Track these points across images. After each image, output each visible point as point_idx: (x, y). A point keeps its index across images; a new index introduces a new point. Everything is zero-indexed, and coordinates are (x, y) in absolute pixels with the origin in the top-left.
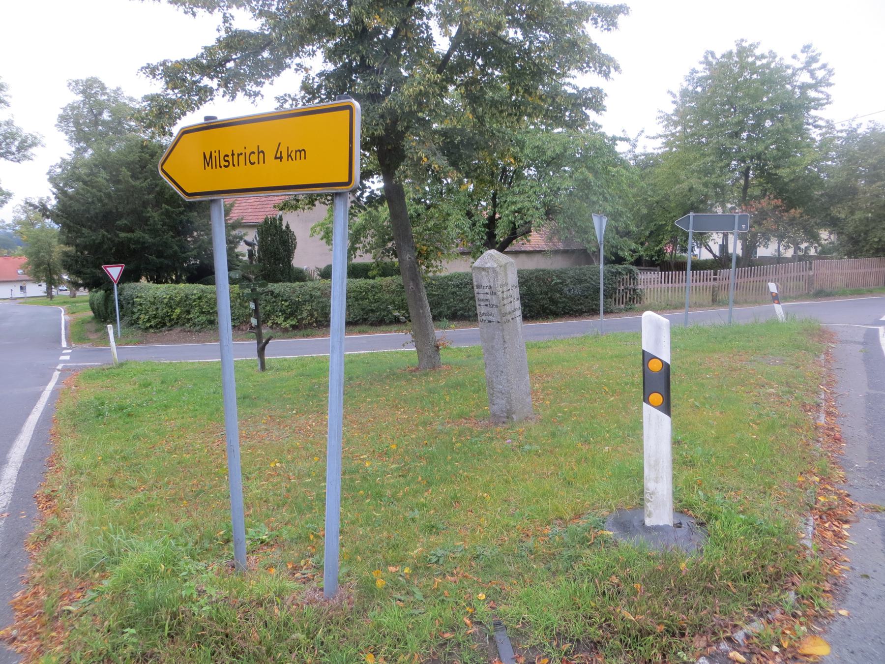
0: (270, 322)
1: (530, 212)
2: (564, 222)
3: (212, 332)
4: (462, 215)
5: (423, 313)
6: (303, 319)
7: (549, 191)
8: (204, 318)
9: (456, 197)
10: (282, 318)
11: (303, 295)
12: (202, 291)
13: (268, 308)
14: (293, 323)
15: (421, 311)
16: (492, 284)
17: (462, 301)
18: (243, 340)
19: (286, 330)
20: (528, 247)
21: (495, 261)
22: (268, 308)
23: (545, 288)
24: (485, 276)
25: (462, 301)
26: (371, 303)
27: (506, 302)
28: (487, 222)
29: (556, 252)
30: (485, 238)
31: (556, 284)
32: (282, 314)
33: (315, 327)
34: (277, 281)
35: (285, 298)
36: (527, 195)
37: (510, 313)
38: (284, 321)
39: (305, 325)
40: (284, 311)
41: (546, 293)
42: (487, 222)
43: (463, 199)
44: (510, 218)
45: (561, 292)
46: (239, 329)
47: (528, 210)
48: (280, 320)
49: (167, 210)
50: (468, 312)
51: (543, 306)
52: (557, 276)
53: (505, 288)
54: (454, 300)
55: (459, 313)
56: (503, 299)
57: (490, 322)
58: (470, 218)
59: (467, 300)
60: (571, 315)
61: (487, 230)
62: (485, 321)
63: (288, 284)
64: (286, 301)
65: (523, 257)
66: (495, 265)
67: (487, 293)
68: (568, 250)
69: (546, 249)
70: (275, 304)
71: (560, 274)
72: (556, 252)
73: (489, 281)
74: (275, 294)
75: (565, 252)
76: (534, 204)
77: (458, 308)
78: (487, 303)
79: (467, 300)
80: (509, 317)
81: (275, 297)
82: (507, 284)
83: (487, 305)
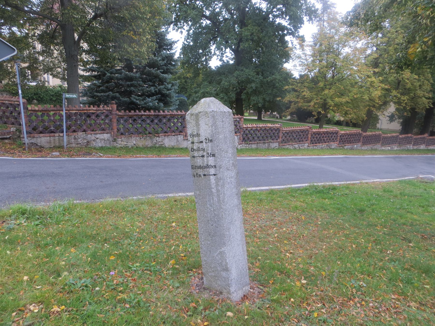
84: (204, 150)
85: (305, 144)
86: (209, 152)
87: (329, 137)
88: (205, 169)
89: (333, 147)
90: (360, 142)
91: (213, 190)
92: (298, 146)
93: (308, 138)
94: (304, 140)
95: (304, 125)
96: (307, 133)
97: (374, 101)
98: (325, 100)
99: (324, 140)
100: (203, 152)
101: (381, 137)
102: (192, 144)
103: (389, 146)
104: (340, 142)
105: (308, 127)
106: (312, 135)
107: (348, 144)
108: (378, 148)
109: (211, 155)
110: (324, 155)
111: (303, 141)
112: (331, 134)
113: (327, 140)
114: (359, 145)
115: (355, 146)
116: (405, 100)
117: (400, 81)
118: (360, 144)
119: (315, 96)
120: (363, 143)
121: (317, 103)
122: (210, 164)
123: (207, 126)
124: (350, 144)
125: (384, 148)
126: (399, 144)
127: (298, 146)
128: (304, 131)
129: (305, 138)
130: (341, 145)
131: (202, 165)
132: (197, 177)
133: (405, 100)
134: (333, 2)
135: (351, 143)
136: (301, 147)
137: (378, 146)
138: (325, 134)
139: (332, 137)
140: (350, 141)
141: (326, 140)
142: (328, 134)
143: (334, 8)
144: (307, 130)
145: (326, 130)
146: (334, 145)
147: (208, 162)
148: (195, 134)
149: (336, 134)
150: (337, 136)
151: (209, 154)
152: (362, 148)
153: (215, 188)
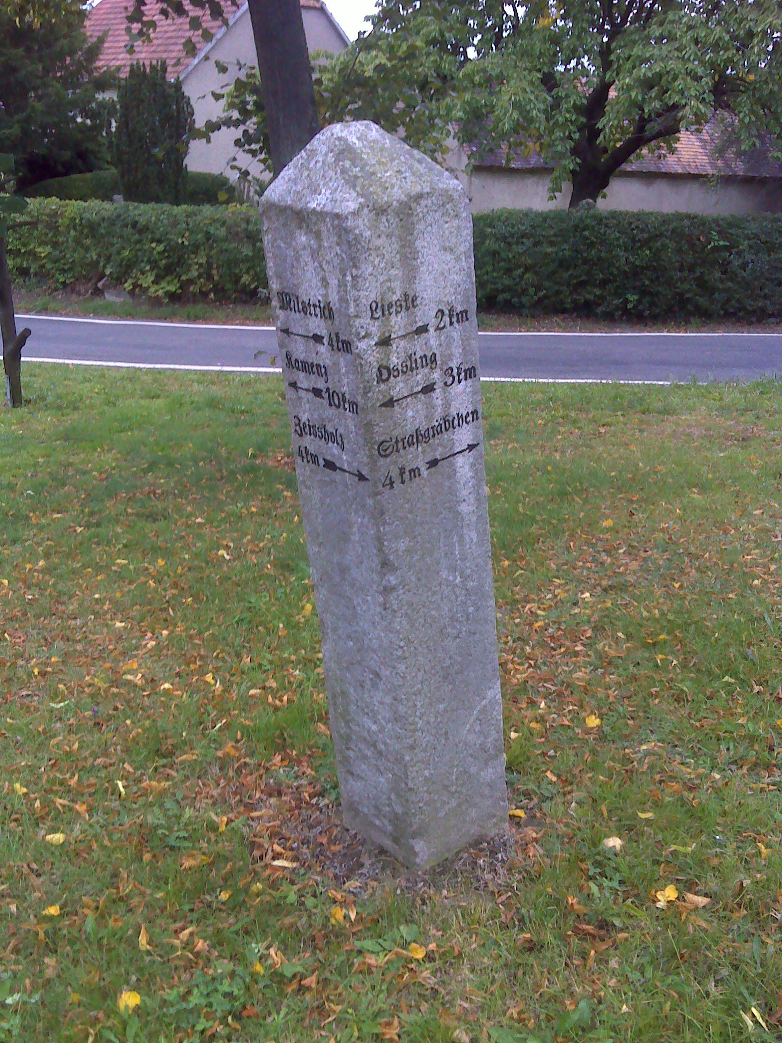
0: (130, 281)
1: (679, 84)
2: (752, 111)
3: (23, 291)
4: (531, 83)
6: (191, 282)
7: (727, 38)
9: (525, 42)
11: (192, 233)
14: (172, 288)
16: (334, 298)
17: (508, 271)
19: (156, 302)
20: (672, 164)
21: (352, 182)
23: (689, 258)
24: (306, 257)
25: (508, 271)
27: (398, 387)
28: (585, 102)
29: (728, 180)
30: (576, 136)
31: (716, 249)
32: (152, 269)
33: (213, 301)
34: (146, 199)
35: (157, 236)
36: (677, 45)
37: (419, 437)
38: (156, 282)
39: (194, 295)
40: (156, 262)
41: (691, 269)
42: (585, 102)
43: (538, 47)
44: (633, 94)
45: (725, 268)
46: (73, 291)
47: (675, 78)
48: (147, 280)
50: (519, 297)
51: (681, 295)
52: (719, 233)
53: (398, 323)
54: (494, 270)
55: (501, 297)
56: (385, 373)
57: (330, 465)
58: (550, 90)
59: (519, 271)
60: (739, 320)
61: (583, 119)
62: (314, 459)
63: (166, 207)
64: (159, 241)
65: (662, 186)
66: (350, 203)
67: (318, 339)
68: (754, 178)
69: (710, 172)
71: (725, 227)
72: (728, 180)
73: (325, 282)
74: (139, 226)
75: (747, 181)
76: (690, 66)
77: (500, 286)
78: (321, 385)
79: (519, 271)
80: (417, 457)
81: (140, 232)
82: (409, 302)
83: (317, 392)
86: (454, 364)
91: (464, 508)
109: (459, 374)
123: (449, 257)
131: (424, 427)
147: (447, 404)
148: (395, 298)
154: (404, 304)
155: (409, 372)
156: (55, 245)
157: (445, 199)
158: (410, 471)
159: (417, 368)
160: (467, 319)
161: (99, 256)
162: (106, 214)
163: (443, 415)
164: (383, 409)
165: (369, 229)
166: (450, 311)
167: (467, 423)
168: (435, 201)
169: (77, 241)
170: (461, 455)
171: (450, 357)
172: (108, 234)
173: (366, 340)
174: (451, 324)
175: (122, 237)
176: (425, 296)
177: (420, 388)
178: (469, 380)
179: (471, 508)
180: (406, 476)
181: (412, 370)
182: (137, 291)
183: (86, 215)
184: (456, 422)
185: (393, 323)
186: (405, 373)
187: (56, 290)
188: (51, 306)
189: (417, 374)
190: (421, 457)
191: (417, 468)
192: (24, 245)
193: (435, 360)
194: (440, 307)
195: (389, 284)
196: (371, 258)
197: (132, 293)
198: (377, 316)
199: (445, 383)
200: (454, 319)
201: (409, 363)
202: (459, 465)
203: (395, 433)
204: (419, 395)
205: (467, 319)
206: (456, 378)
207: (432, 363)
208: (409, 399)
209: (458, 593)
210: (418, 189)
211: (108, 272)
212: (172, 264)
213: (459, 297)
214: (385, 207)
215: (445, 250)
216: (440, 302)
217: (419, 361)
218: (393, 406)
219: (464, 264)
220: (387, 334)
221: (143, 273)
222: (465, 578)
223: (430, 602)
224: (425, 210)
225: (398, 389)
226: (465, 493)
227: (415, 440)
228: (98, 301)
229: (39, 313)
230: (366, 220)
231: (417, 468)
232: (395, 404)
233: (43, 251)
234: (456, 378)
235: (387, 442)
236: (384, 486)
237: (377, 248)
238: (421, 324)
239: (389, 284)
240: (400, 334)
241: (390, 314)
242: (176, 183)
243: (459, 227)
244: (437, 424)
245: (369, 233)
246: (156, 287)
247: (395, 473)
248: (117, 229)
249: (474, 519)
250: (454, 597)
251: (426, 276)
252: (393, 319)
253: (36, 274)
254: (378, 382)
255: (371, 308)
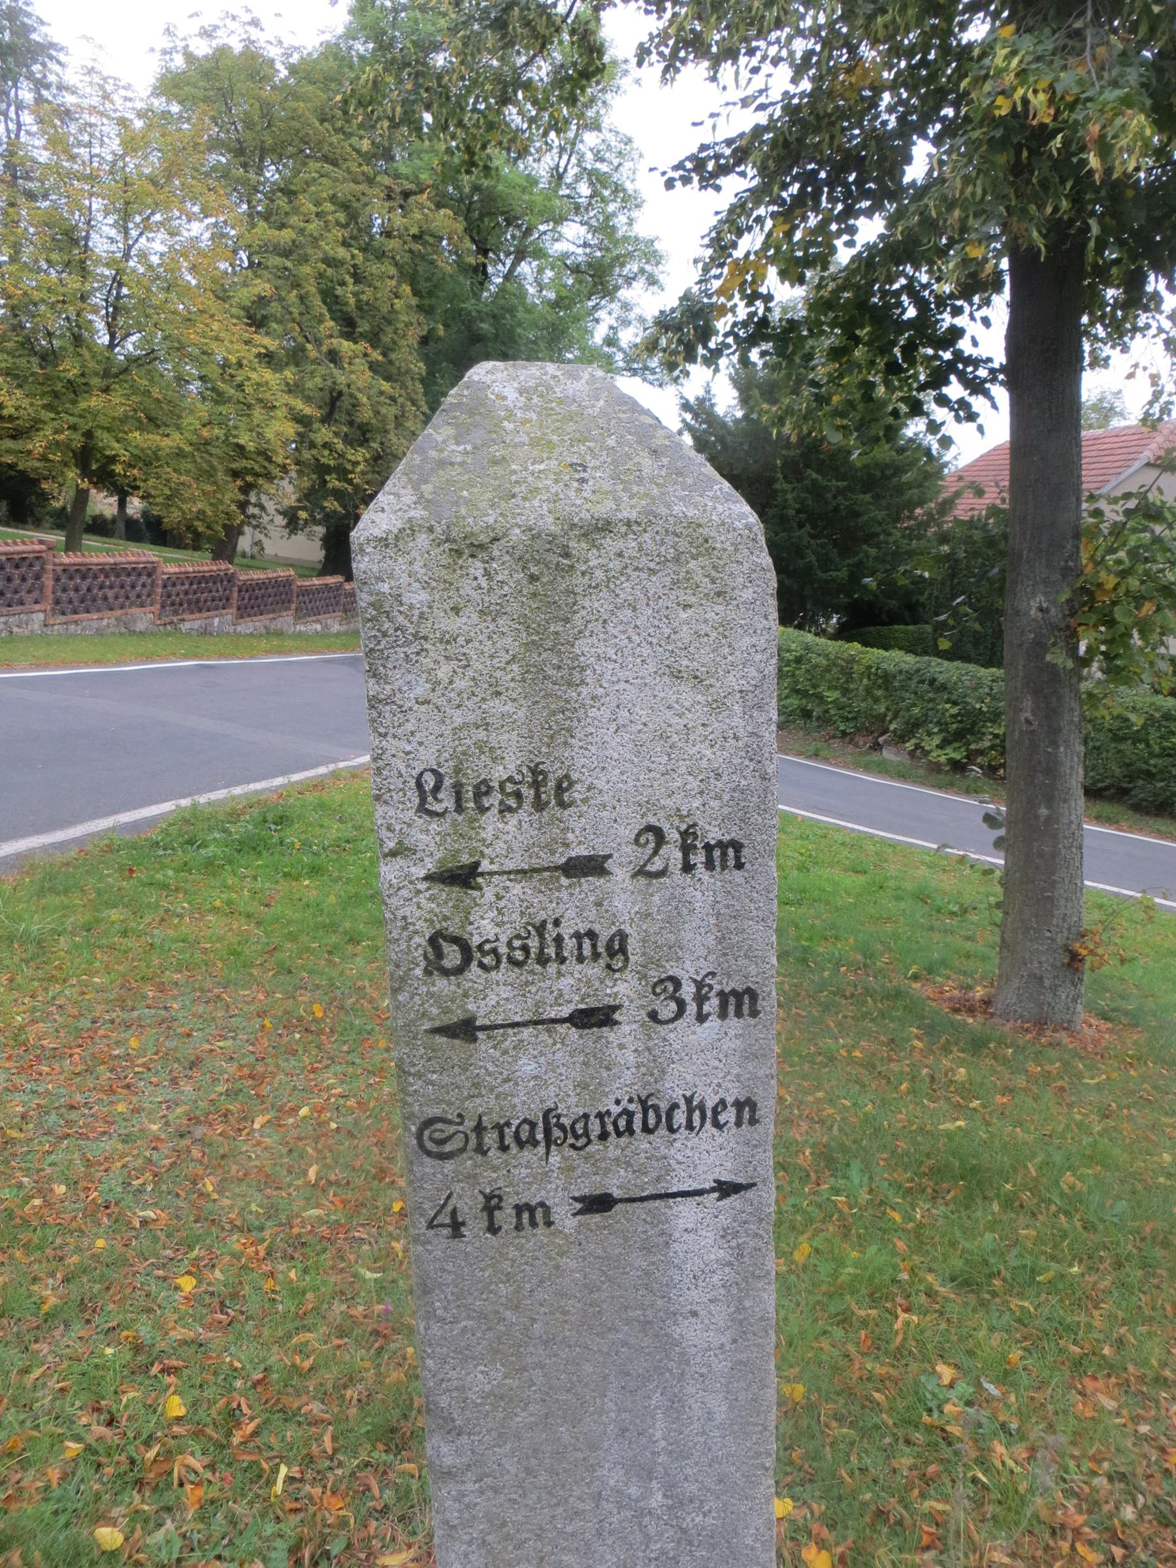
0: (913, 741)
5: (1049, 820)
8: (796, 702)
10: (937, 740)
12: (807, 648)
13: (916, 710)
14: (957, 756)
15: (1044, 811)
18: (846, 766)
19: (935, 768)
22: (916, 710)
26: (1152, 755)
32: (940, 731)
35: (954, 698)
38: (940, 747)
49: (814, 482)
63: (972, 667)
64: (955, 703)
70: (930, 705)
84: (618, 947)
85: (34, 616)
86: (687, 971)
87: (122, 587)
88: (614, 1148)
89: (140, 626)
90: (231, 606)
91: (691, 1333)
92: (5, 623)
93: (42, 588)
94: (29, 599)
95: (8, 535)
96: (37, 568)
97: (269, 459)
98: (89, 435)
99: (105, 598)
100: (594, 970)
101: (294, 587)
102: (442, 892)
103: (318, 621)
104: (163, 607)
105: (41, 542)
106: (58, 579)
107: (192, 612)
108: (285, 627)
109: (700, 999)
110: (119, 663)
111: (22, 603)
112: (129, 575)
113: (116, 598)
114: (229, 617)
115: (216, 621)
116: (358, 463)
117: (340, 394)
118: (230, 614)
119: (47, 415)
120: (239, 608)
121: (57, 443)
122: (678, 1095)
123: (687, 695)
124: (197, 615)
125: (303, 628)
126: (345, 611)
127: (5, 623)
128: (24, 559)
129: (29, 592)
130: (168, 620)
131: (571, 1109)
132: (493, 1229)
133: (358, 463)
134: (55, 40)
135: (200, 611)
136: (15, 629)
137: (285, 621)
138: (107, 577)
139: (133, 587)
140: (198, 601)
141: (111, 600)
142: (118, 576)
143: (59, 63)
144: (37, 558)
145: (112, 560)
146: (143, 618)
147: (655, 1068)
148: (499, 773)
149: (149, 575)
150: (153, 584)
151: (688, 991)
152: (239, 628)
153: (721, 1314)
154: (528, 793)
155: (532, 964)
156: (845, 691)
157: (683, 545)
158: (519, 1209)
159: (562, 960)
160: (739, 866)
161: (888, 709)
162: (905, 667)
163: (638, 1089)
164: (441, 1040)
165: (426, 586)
166: (684, 834)
167: (717, 1125)
168: (650, 545)
169: (868, 691)
170: (691, 1202)
171: (675, 950)
172: (902, 688)
173: (400, 861)
174: (688, 868)
175: (916, 693)
176: (600, 784)
177: (566, 1011)
178: (733, 1022)
179: (715, 1339)
180: (506, 1216)
181: (543, 960)
182: (919, 752)
183: (884, 666)
184: (680, 1117)
185: (488, 834)
186: (518, 964)
187: (834, 737)
188: (824, 753)
189: (560, 974)
190: (558, 1180)
191: (542, 1204)
192: (814, 687)
193: (623, 950)
194: (653, 820)
195: (481, 734)
196: (427, 662)
197: (912, 754)
198: (438, 808)
199: (653, 1016)
200: (699, 858)
201: (534, 943)
202: (681, 1224)
203: (474, 1107)
204: (562, 1029)
205: (739, 866)
206: (692, 1008)
207: (612, 954)
208: (526, 1032)
209: (652, 1529)
210: (604, 509)
211: (892, 727)
212: (963, 729)
213: (715, 804)
214: (483, 538)
215: (677, 676)
216: (650, 805)
217: (570, 944)
218: (475, 1040)
219: (737, 721)
220: (466, 859)
221: (929, 734)
222: (677, 1503)
223: (561, 1532)
224: (616, 565)
225: (492, 999)
226: (695, 1296)
227: (540, 1136)
228: (875, 757)
229: (809, 757)
230: (417, 566)
231: (542, 1204)
232: (481, 1035)
233: (832, 695)
234: (692, 1008)
235: (450, 1122)
236: (431, 1226)
237: (447, 640)
238: (582, 851)
239: (481, 734)
240: (510, 865)
241: (483, 810)
242: (993, 645)
243: (724, 626)
244: (616, 1110)
245: (423, 596)
246: (940, 752)
247: (468, 1204)
248: (913, 684)
249: (721, 1366)
250: (639, 1537)
251: (607, 734)
252: (490, 823)
253: (818, 718)
254: (428, 972)
255: (419, 785)
